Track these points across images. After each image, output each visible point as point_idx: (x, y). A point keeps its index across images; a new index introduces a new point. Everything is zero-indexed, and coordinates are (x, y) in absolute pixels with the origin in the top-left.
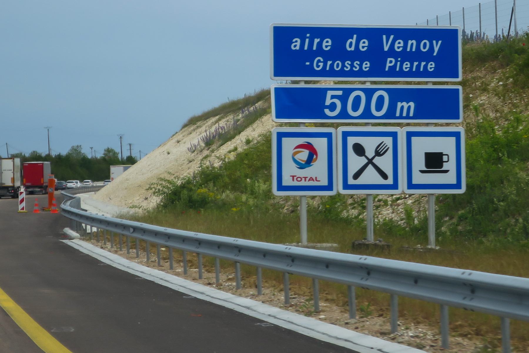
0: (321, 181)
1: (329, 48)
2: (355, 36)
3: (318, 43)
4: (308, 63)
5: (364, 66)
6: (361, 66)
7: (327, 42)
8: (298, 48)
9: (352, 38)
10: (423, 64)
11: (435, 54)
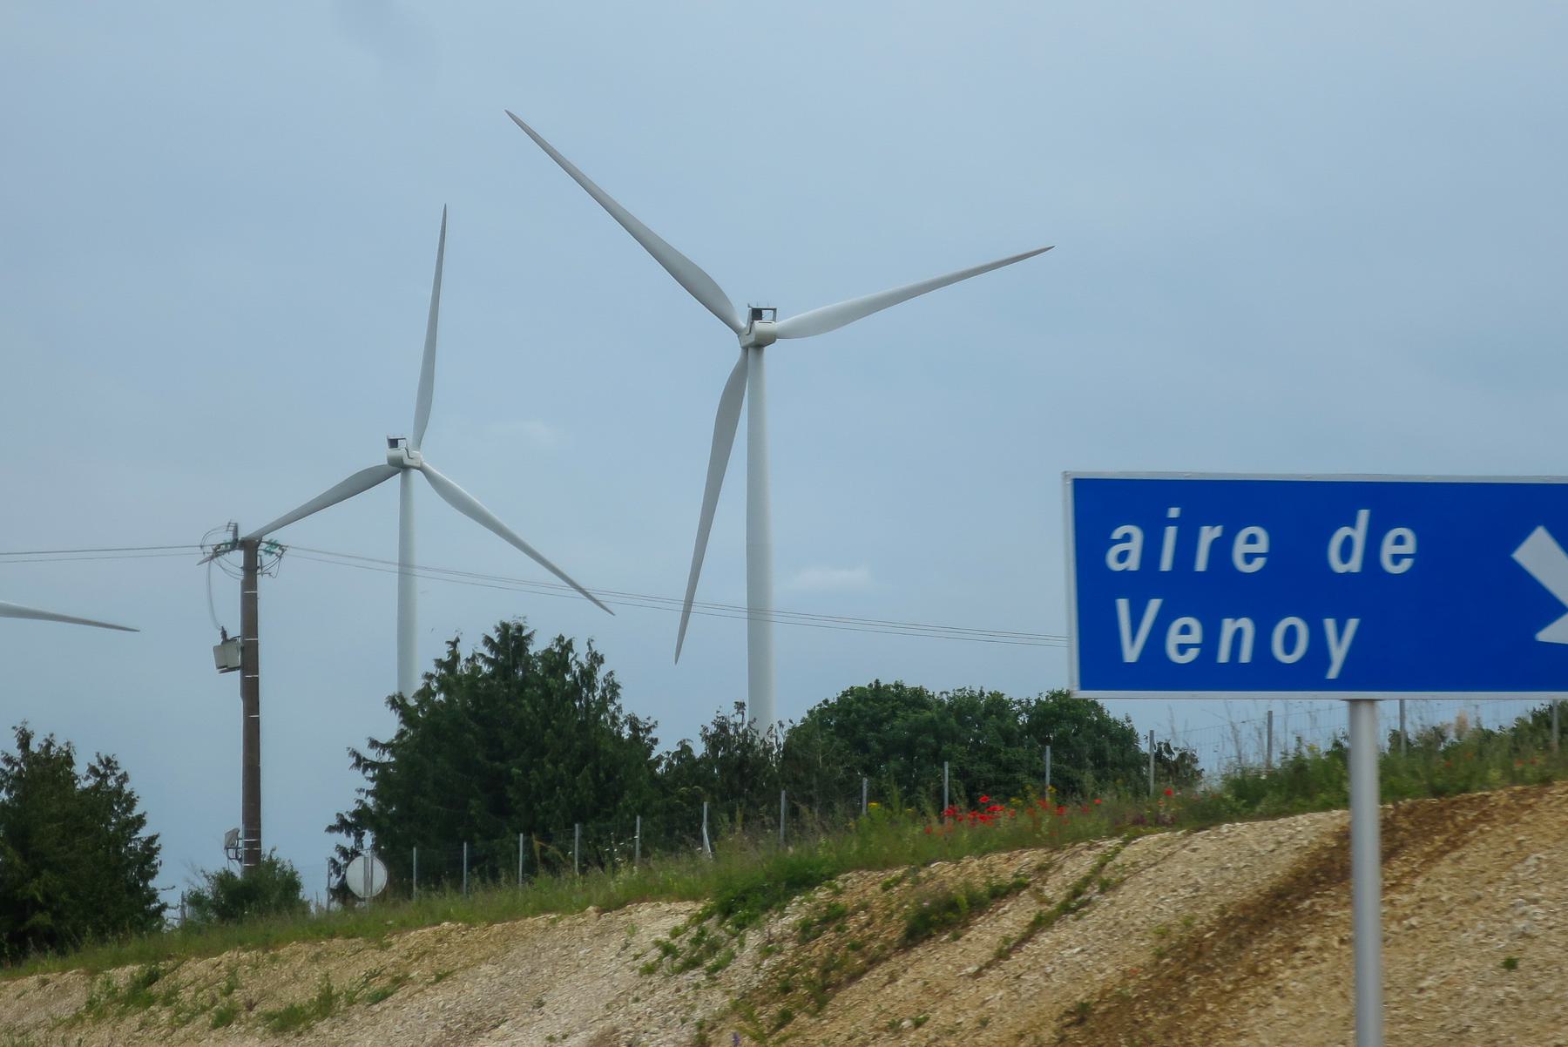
1: (1259, 564)
2: (1363, 516)
3: (1215, 544)
7: (1252, 539)
8: (1133, 563)
9: (1352, 523)
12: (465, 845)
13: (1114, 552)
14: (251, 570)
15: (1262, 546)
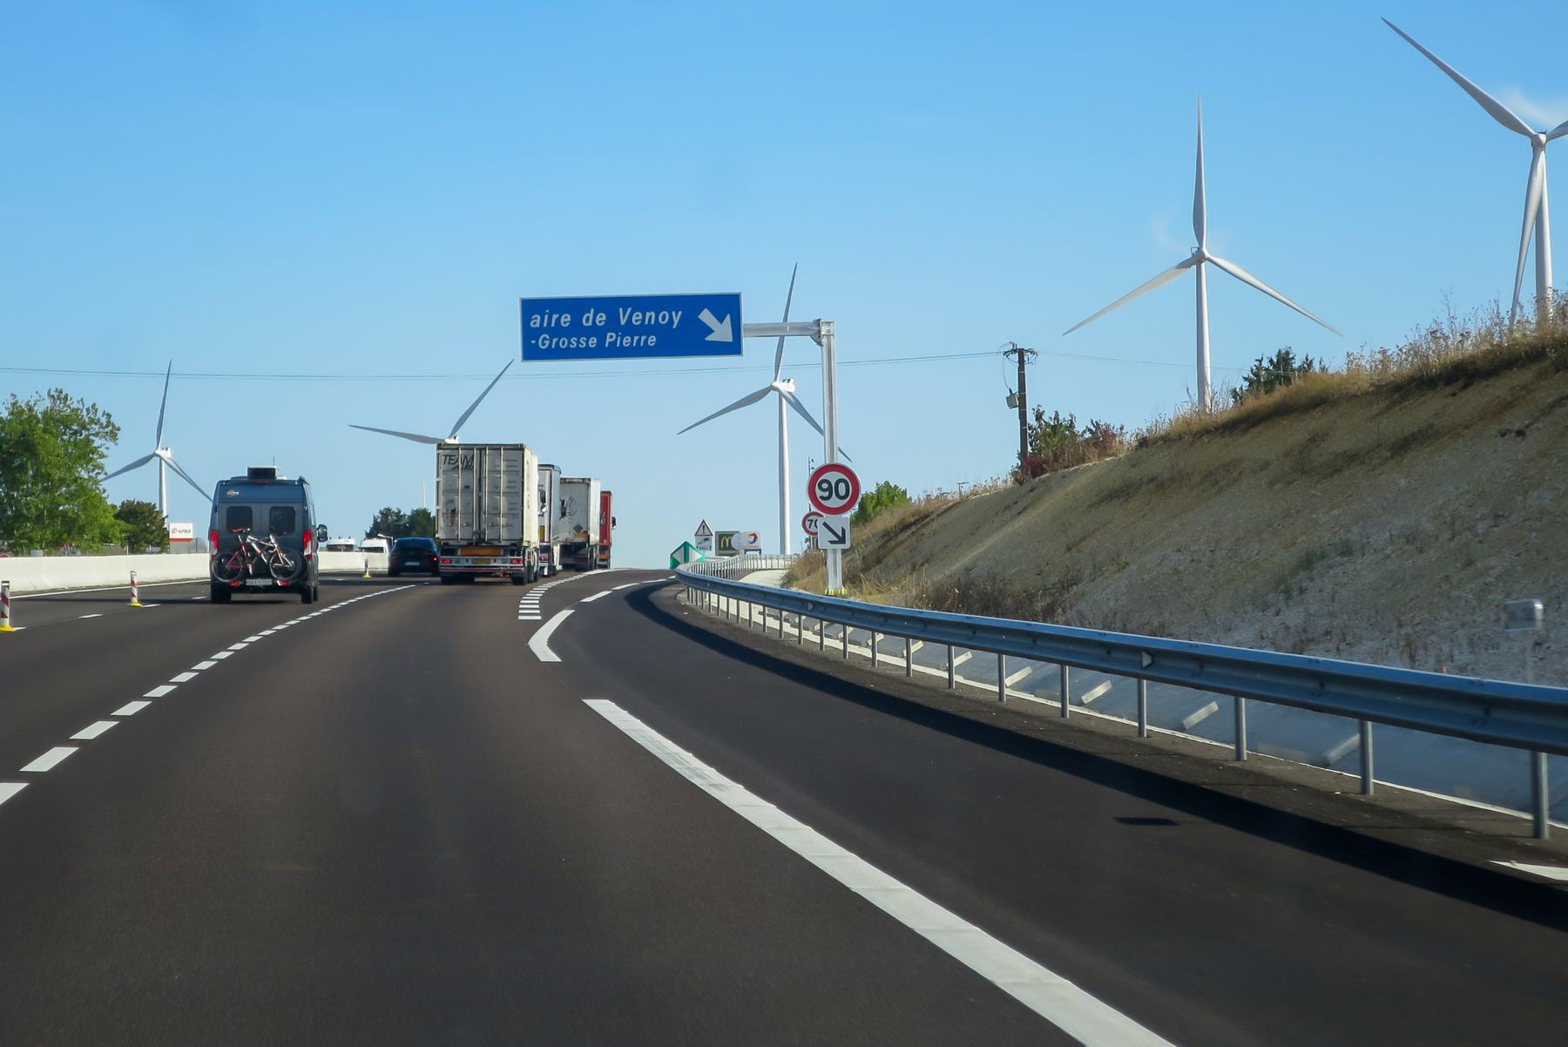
0: (1056, 409)
2: (592, 310)
4: (533, 342)
5: (590, 342)
6: (587, 342)
8: (538, 325)
9: (589, 313)
10: (643, 338)
11: (674, 327)
12: (606, 708)
13: (532, 322)
14: (1021, 362)
15: (569, 319)
